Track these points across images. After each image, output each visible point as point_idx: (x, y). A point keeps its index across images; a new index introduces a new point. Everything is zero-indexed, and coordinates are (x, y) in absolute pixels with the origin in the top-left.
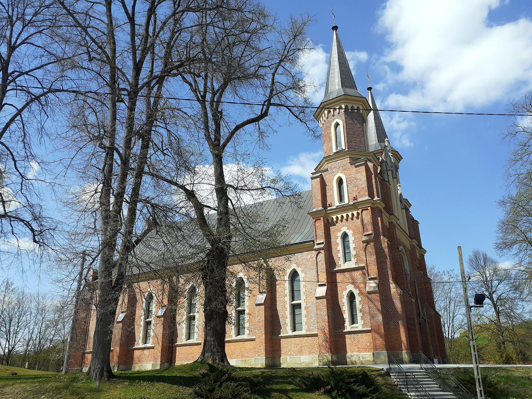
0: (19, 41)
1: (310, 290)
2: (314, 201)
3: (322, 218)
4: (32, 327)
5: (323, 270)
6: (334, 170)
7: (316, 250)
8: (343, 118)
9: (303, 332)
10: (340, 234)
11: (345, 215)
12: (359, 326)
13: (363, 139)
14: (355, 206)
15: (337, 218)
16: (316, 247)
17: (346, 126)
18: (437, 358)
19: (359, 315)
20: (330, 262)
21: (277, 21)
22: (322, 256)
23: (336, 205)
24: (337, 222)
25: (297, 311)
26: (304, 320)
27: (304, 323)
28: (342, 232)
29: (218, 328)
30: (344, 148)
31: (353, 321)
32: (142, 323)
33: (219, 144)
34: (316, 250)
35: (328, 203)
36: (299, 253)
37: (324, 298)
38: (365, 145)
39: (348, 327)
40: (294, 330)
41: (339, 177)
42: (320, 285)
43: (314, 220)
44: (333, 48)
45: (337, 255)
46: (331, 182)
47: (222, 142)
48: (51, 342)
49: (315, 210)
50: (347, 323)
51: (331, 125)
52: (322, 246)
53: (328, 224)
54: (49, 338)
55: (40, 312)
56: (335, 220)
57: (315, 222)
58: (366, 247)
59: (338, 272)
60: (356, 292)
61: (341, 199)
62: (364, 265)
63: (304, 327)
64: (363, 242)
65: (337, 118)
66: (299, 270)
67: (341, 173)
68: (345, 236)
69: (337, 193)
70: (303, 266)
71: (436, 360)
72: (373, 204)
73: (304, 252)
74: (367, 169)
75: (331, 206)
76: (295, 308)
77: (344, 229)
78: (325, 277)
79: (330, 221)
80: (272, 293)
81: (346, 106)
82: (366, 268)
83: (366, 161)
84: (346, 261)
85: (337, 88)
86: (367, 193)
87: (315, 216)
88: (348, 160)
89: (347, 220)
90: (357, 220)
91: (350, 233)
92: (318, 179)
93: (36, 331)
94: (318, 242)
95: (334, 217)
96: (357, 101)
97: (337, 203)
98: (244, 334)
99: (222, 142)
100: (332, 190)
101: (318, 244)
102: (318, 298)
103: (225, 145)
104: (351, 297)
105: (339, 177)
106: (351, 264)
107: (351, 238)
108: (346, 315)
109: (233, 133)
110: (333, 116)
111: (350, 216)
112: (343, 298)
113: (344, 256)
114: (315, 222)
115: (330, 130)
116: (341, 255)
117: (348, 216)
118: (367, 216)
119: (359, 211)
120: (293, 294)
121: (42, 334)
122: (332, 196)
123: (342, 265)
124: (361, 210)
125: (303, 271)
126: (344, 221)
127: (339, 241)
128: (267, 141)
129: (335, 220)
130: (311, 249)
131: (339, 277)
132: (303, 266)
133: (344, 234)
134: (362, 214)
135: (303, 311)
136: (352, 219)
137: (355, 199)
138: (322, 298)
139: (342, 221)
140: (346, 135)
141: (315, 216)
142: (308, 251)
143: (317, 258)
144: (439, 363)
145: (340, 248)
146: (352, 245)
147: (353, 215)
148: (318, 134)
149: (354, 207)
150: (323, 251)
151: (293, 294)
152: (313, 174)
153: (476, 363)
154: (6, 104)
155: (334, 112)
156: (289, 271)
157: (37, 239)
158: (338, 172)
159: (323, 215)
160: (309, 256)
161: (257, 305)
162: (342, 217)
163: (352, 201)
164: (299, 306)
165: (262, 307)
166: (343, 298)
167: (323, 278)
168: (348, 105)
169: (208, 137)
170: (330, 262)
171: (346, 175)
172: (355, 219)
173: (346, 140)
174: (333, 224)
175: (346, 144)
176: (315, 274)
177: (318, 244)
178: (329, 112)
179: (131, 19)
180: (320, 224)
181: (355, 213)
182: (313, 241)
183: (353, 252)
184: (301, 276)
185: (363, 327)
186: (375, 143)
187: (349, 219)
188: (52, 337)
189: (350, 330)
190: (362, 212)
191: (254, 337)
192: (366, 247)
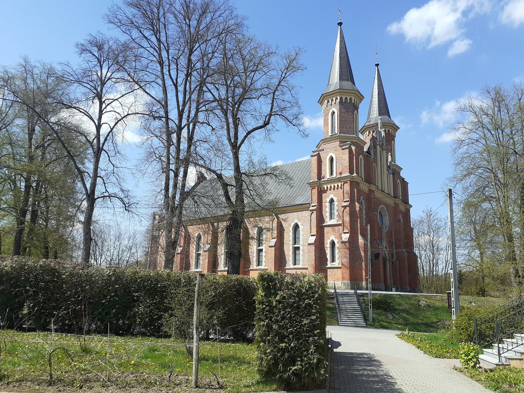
0: (106, 79)
1: (306, 238)
2: (312, 174)
3: (316, 188)
4: (112, 251)
5: (315, 225)
6: (328, 150)
7: (311, 211)
8: (338, 107)
9: (300, 266)
10: (328, 200)
11: (332, 186)
12: (336, 264)
13: (353, 124)
14: (338, 180)
15: (327, 187)
16: (311, 208)
17: (340, 114)
18: (394, 288)
19: (337, 256)
20: (320, 219)
21: (279, 48)
22: (314, 215)
23: (327, 178)
24: (327, 190)
25: (297, 252)
26: (301, 258)
27: (301, 260)
28: (330, 198)
29: (235, 264)
30: (337, 132)
31: (333, 260)
32: (194, 255)
33: (237, 144)
34: (311, 211)
35: (322, 176)
36: (300, 211)
37: (313, 244)
38: (354, 130)
39: (329, 265)
40: (295, 264)
41: (331, 156)
42: (312, 235)
43: (311, 188)
44: (337, 41)
45: (326, 215)
46: (325, 160)
47: (238, 144)
48: (127, 263)
49: (311, 181)
50: (329, 263)
51: (329, 113)
52: (315, 208)
53: (321, 192)
54: (126, 259)
55: (118, 239)
56: (326, 189)
57: (312, 189)
58: (344, 210)
59: (325, 227)
60: (336, 241)
61: (332, 174)
62: (341, 223)
63: (301, 263)
64: (342, 207)
65: (334, 107)
66: (299, 224)
67: (333, 153)
68: (332, 201)
69: (329, 166)
70: (302, 221)
71: (394, 289)
72: (352, 179)
73: (303, 211)
74: (350, 152)
75: (324, 178)
76: (296, 249)
77: (332, 196)
78: (316, 230)
79: (322, 189)
80: (281, 239)
81: (341, 98)
82: (342, 225)
83: (351, 145)
84: (331, 219)
85: (336, 81)
86: (348, 170)
87: (312, 185)
88: (338, 143)
89: (334, 189)
90: (341, 190)
91: (335, 199)
92: (316, 157)
93: (115, 253)
94: (313, 205)
95: (325, 187)
96: (350, 93)
97: (328, 176)
98: (262, 265)
99: (238, 144)
100: (326, 165)
101: (313, 206)
102: (309, 244)
103: (240, 146)
104: (333, 244)
105: (331, 156)
106: (334, 222)
107: (336, 203)
108: (329, 256)
109: (249, 133)
110: (331, 105)
111: (336, 187)
112: (327, 244)
113: (330, 215)
114: (312, 189)
115: (328, 117)
116: (328, 214)
117: (334, 186)
118: (347, 187)
119: (342, 183)
120: (295, 240)
121: (120, 256)
122: (325, 170)
123: (328, 222)
124: (343, 183)
125: (302, 225)
126: (332, 190)
127: (328, 204)
128: (272, 137)
129: (326, 189)
130: (307, 209)
131: (326, 230)
132: (302, 221)
133: (331, 199)
134: (343, 186)
135: (301, 252)
136: (338, 189)
137: (341, 174)
138: (312, 245)
139: (330, 190)
140: (339, 122)
141: (312, 185)
142: (306, 210)
143: (311, 216)
144: (396, 291)
145: (328, 209)
146: (336, 208)
147: (338, 186)
148: (307, 133)
149: (338, 180)
150: (315, 212)
151: (295, 240)
152: (313, 152)
153: (370, 290)
154: (103, 124)
155: (332, 102)
156: (293, 224)
157: (127, 209)
158: (330, 152)
159: (318, 185)
160: (307, 213)
161: (270, 247)
162: (331, 187)
163: (338, 175)
164: (298, 248)
165: (273, 248)
166: (327, 244)
167: (314, 232)
168: (342, 97)
169: (229, 139)
170: (320, 219)
171: (336, 155)
172: (339, 189)
173: (339, 126)
174: (325, 191)
175: (339, 129)
176: (309, 227)
177: (313, 206)
178: (328, 101)
179: (176, 85)
180: (315, 191)
181: (340, 184)
182: (309, 204)
183: (336, 213)
184: (301, 227)
185: (338, 265)
186: (376, 116)
187: (336, 189)
188: (128, 258)
189: (330, 266)
190: (344, 184)
191: (268, 268)
192: (344, 210)
